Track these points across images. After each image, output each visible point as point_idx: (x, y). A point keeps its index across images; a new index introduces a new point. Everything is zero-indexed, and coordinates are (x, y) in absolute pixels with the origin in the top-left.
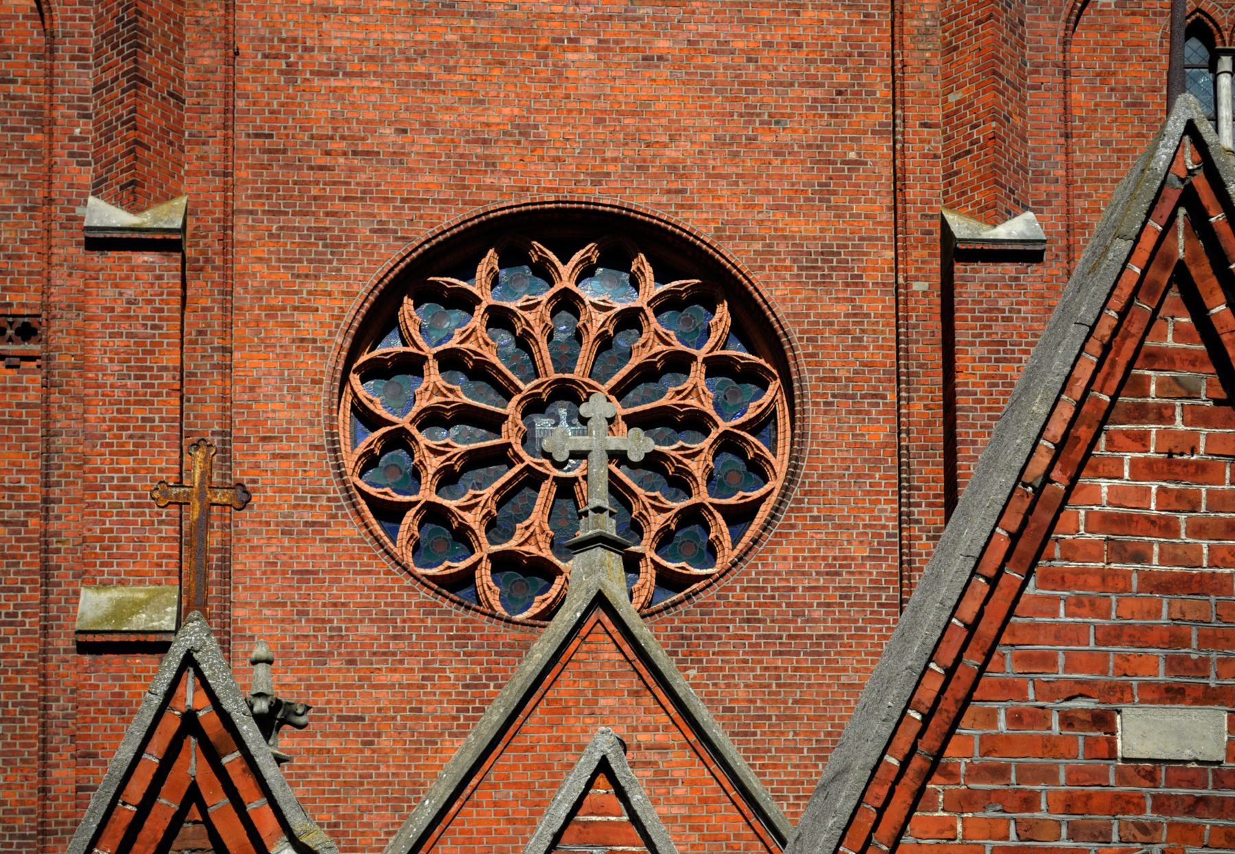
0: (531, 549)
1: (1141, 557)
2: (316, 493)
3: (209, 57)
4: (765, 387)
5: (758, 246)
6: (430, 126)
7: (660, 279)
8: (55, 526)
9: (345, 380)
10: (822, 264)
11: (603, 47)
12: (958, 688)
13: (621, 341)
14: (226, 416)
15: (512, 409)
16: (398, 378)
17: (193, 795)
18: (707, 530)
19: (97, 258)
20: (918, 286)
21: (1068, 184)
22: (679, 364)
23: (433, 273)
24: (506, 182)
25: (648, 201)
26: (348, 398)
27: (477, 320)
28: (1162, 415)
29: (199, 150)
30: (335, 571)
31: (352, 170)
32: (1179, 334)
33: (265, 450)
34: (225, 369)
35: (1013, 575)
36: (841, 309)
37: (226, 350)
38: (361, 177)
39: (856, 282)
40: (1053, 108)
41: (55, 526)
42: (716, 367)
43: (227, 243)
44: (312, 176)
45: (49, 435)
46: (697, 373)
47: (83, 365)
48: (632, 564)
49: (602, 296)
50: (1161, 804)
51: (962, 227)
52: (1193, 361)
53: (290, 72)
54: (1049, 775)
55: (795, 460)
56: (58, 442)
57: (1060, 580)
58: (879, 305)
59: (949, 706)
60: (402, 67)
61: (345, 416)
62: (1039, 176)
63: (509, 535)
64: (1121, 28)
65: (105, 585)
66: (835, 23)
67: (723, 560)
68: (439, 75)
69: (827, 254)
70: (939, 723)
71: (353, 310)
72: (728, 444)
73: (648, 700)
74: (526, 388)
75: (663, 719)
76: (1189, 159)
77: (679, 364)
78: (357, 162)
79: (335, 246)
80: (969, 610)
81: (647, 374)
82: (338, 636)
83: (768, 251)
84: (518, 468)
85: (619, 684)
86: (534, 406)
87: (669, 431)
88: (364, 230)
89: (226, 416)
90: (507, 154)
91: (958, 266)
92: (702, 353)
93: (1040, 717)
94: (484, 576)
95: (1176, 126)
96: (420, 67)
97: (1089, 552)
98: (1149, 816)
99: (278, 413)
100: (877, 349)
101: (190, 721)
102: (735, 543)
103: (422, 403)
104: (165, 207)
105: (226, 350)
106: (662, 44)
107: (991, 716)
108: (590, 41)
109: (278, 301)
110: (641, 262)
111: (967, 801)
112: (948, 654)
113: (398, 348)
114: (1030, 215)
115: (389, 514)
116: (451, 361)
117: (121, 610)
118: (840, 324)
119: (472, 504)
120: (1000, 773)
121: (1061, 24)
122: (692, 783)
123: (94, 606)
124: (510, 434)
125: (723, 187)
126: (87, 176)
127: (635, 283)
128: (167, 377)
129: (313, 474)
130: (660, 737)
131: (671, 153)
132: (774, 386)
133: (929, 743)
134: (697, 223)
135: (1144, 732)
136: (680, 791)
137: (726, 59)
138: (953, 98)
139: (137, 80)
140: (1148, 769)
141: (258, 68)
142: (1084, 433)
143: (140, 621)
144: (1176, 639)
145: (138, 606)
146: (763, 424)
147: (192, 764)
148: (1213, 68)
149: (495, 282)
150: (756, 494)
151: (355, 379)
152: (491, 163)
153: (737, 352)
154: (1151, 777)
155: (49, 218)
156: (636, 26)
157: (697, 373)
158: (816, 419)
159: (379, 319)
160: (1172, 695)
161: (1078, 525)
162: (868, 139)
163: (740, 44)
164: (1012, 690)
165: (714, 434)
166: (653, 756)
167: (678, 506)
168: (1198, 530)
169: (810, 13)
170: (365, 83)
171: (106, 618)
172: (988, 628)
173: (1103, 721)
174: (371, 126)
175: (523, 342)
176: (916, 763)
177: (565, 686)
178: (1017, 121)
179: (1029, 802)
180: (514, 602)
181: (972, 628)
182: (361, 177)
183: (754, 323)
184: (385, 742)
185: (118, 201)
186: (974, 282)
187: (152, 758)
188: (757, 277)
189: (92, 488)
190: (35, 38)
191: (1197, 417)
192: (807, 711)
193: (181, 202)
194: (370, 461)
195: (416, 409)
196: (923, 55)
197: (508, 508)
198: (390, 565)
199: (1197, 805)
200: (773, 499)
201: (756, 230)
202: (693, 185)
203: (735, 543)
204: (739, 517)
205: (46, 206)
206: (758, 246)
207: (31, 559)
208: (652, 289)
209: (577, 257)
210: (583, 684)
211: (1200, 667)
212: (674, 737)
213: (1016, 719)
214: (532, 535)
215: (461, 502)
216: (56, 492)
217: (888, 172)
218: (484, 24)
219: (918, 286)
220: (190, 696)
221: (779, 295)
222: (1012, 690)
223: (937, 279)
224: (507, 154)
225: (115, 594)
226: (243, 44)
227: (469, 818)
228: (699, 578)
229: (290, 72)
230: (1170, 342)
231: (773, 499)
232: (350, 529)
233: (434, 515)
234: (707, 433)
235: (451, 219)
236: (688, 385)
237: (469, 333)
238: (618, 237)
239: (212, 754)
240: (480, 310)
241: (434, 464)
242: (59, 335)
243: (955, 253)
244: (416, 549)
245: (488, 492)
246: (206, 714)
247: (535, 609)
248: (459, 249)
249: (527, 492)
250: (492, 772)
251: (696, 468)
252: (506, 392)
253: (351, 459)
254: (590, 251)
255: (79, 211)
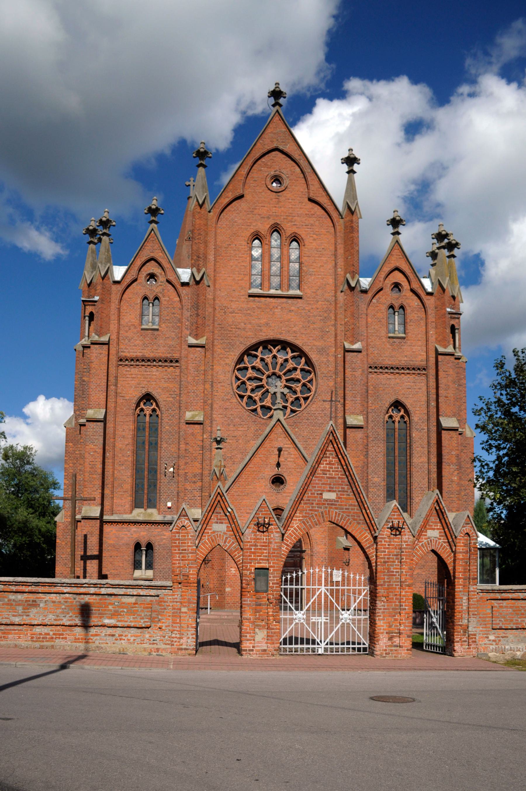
0: (267, 404)
1: (326, 474)
2: (229, 393)
3: (210, 310)
4: (311, 373)
5: (310, 347)
6: (250, 323)
7: (292, 352)
8: (181, 399)
9: (234, 371)
10: (321, 351)
11: (282, 308)
12: (304, 491)
13: (284, 364)
14: (212, 378)
15: (264, 377)
16: (243, 371)
17: (219, 501)
18: (300, 401)
19: (190, 349)
20: (339, 356)
21: (367, 337)
22: (295, 369)
23: (250, 351)
24: (264, 334)
25: (290, 338)
26: (234, 375)
27: (258, 360)
28: (329, 457)
29: (208, 328)
30: (232, 408)
31: (236, 331)
32: (331, 448)
33: (219, 385)
34: (212, 369)
35: (311, 477)
36: (325, 360)
37: (213, 366)
38: (238, 333)
39: (328, 354)
40: (364, 322)
41: (181, 399)
42: (302, 370)
43: (213, 345)
44: (228, 332)
45: (181, 381)
46: (299, 371)
47: (187, 368)
48: (285, 414)
49: (281, 357)
50: (328, 504)
51: (348, 346)
52: (332, 451)
53: (225, 312)
54: (315, 501)
55: (316, 388)
56: (182, 383)
57: (317, 477)
58: (332, 359)
59: (303, 493)
60: (245, 312)
61: (234, 378)
62: (362, 335)
63: (263, 401)
64: (378, 307)
65: (191, 411)
66: (325, 304)
67: (303, 406)
68: (252, 313)
69: (322, 349)
70: (302, 495)
71: (236, 358)
72: (304, 385)
73: (287, 439)
74: (267, 373)
75: (289, 442)
76: (332, 428)
77: (295, 369)
78: (237, 330)
79: (233, 346)
80: (306, 481)
81: (289, 371)
82: (232, 421)
83: (312, 348)
84: (265, 389)
85: (282, 436)
86: (269, 377)
87: (293, 382)
88: (238, 343)
89: (212, 378)
90: (264, 329)
91: (346, 353)
92: (299, 367)
93: (314, 494)
94: (259, 409)
95: (330, 425)
96: (249, 312)
97: (320, 474)
98: (326, 506)
99: (222, 377)
100: (332, 368)
101: (219, 493)
102: (305, 404)
103: (248, 376)
104: (202, 339)
105: (213, 366)
106: (293, 308)
107: (308, 493)
108: (279, 307)
109: (222, 356)
110: (288, 350)
111: (305, 504)
112: (303, 487)
113: (244, 365)
114: (360, 343)
115: (242, 397)
116: (253, 368)
117: (194, 416)
118: (324, 362)
119: (257, 396)
120: (309, 500)
121: (366, 306)
122: (294, 455)
123: (189, 415)
124: (264, 382)
125: (303, 336)
126: (188, 332)
127: (287, 353)
128: (202, 372)
129: (228, 389)
130: (289, 446)
131: (294, 329)
132: (313, 374)
133: (301, 497)
134: (298, 342)
135: (327, 496)
136: (292, 456)
137: (305, 311)
138: (346, 320)
139: (198, 315)
140: (326, 500)
141: (219, 312)
142: (319, 460)
143: (197, 419)
144: (330, 484)
145: (196, 415)
146: (310, 381)
147: (219, 498)
148: (394, 314)
149: (262, 352)
150: (309, 395)
151: (236, 371)
152: (261, 330)
153: (307, 368)
154: (327, 501)
155: (181, 340)
156: (288, 305)
157: (299, 371)
158: (320, 381)
159: (241, 360)
160: (329, 491)
161: (319, 471)
162: (330, 327)
163: (307, 308)
164: (311, 490)
165: (301, 383)
166: (288, 449)
167: (295, 396)
168: (333, 471)
169: (320, 303)
170: (238, 315)
171: (191, 418)
172: (308, 484)
173: (321, 494)
174: (239, 323)
175: (267, 364)
176: (300, 499)
177: (272, 436)
178: (358, 324)
179: (313, 504)
180: (264, 415)
181: (306, 484)
182: (238, 333)
183: (309, 362)
184: (240, 441)
185: (194, 338)
186: (349, 356)
187: (215, 497)
188: (310, 353)
189: (189, 392)
190: (179, 305)
191: (333, 458)
192: (317, 437)
193: (205, 338)
194: (238, 387)
195: (247, 377)
196: (341, 311)
197: (263, 396)
198: (242, 407)
199: (332, 504)
200: (312, 396)
201: (309, 344)
202: (298, 335)
203: (305, 404)
204: (306, 399)
205: (181, 338)
206: (310, 347)
207: (177, 405)
208: (290, 354)
209: (277, 348)
210: (275, 436)
211: (333, 488)
212: (291, 446)
213: (311, 494)
214: (267, 402)
215: (255, 395)
216: (182, 392)
217: (334, 333)
218: (260, 304)
219: (339, 356)
220: (219, 490)
221: (314, 357)
222: (311, 490)
223: (343, 354)
224: (264, 329)
225: (192, 413)
226: (217, 307)
227: (255, 460)
228: (298, 411)
229: (225, 312)
230: (330, 449)
231: (312, 396)
232: (235, 400)
233: (250, 397)
234: (300, 382)
235: (254, 341)
236: (296, 373)
237: (257, 363)
238: (284, 345)
239: (221, 497)
240: (259, 358)
241: (250, 388)
242: (183, 362)
243: (346, 351)
244: (247, 403)
245: (260, 393)
246: (220, 492)
247: (268, 416)
248: (255, 347)
249: (267, 393)
250: (259, 452)
251: (298, 389)
252: (263, 374)
253: (235, 386)
254: (279, 347)
255: (187, 339)
